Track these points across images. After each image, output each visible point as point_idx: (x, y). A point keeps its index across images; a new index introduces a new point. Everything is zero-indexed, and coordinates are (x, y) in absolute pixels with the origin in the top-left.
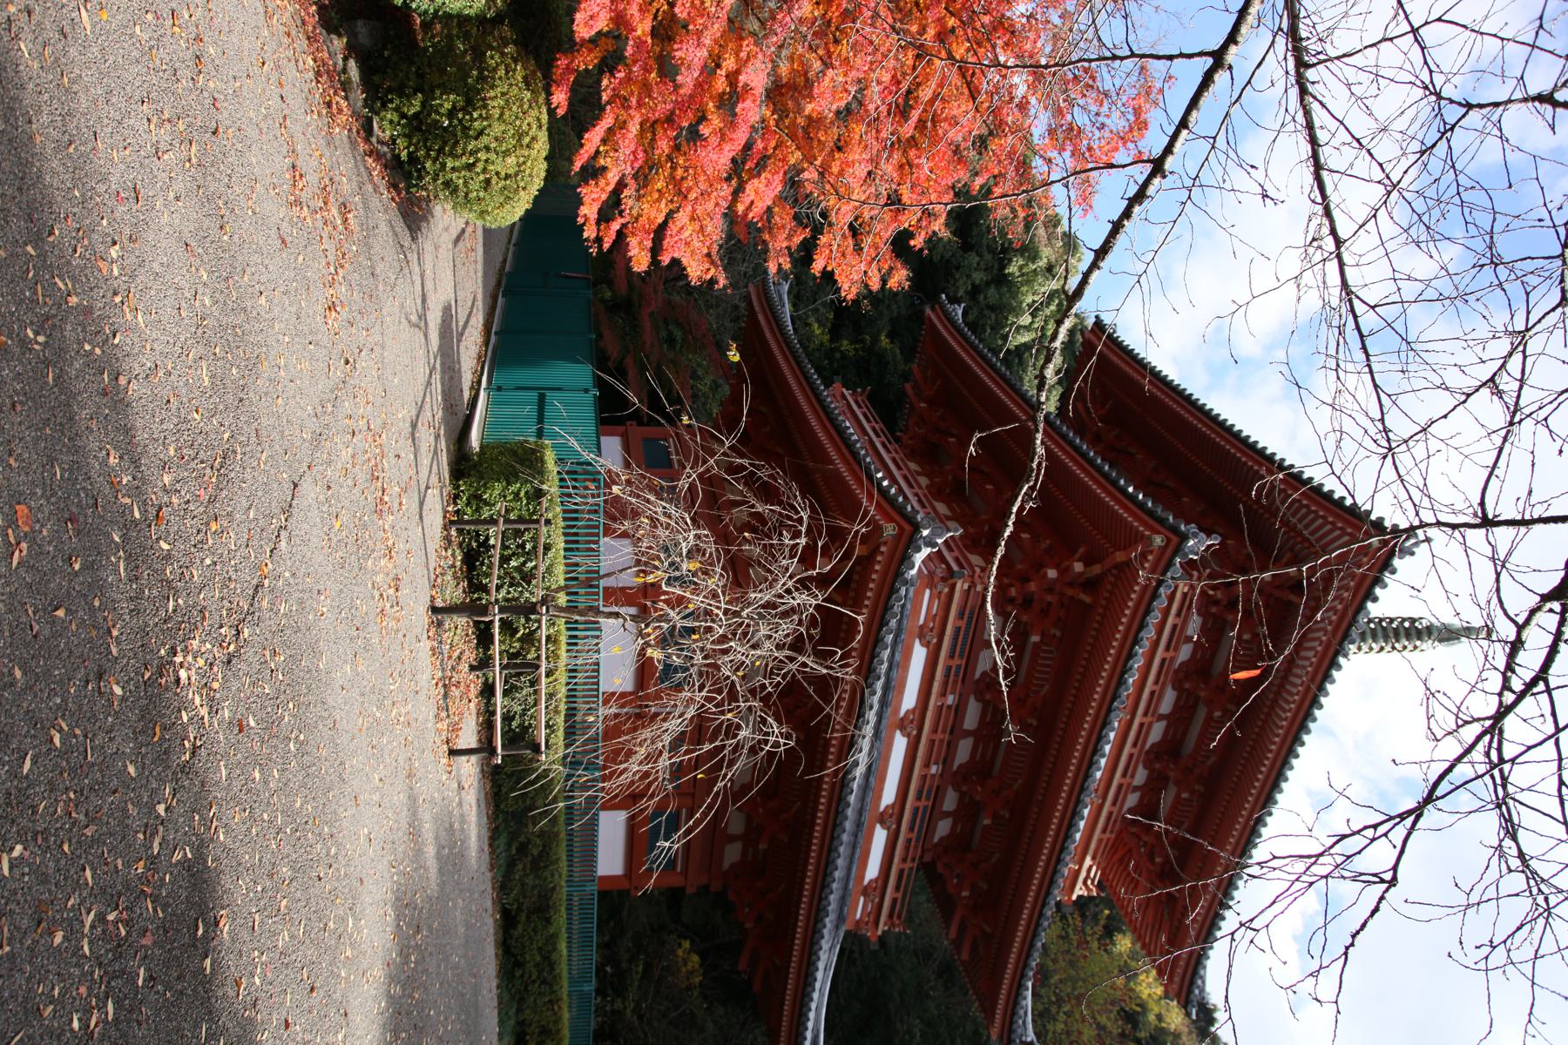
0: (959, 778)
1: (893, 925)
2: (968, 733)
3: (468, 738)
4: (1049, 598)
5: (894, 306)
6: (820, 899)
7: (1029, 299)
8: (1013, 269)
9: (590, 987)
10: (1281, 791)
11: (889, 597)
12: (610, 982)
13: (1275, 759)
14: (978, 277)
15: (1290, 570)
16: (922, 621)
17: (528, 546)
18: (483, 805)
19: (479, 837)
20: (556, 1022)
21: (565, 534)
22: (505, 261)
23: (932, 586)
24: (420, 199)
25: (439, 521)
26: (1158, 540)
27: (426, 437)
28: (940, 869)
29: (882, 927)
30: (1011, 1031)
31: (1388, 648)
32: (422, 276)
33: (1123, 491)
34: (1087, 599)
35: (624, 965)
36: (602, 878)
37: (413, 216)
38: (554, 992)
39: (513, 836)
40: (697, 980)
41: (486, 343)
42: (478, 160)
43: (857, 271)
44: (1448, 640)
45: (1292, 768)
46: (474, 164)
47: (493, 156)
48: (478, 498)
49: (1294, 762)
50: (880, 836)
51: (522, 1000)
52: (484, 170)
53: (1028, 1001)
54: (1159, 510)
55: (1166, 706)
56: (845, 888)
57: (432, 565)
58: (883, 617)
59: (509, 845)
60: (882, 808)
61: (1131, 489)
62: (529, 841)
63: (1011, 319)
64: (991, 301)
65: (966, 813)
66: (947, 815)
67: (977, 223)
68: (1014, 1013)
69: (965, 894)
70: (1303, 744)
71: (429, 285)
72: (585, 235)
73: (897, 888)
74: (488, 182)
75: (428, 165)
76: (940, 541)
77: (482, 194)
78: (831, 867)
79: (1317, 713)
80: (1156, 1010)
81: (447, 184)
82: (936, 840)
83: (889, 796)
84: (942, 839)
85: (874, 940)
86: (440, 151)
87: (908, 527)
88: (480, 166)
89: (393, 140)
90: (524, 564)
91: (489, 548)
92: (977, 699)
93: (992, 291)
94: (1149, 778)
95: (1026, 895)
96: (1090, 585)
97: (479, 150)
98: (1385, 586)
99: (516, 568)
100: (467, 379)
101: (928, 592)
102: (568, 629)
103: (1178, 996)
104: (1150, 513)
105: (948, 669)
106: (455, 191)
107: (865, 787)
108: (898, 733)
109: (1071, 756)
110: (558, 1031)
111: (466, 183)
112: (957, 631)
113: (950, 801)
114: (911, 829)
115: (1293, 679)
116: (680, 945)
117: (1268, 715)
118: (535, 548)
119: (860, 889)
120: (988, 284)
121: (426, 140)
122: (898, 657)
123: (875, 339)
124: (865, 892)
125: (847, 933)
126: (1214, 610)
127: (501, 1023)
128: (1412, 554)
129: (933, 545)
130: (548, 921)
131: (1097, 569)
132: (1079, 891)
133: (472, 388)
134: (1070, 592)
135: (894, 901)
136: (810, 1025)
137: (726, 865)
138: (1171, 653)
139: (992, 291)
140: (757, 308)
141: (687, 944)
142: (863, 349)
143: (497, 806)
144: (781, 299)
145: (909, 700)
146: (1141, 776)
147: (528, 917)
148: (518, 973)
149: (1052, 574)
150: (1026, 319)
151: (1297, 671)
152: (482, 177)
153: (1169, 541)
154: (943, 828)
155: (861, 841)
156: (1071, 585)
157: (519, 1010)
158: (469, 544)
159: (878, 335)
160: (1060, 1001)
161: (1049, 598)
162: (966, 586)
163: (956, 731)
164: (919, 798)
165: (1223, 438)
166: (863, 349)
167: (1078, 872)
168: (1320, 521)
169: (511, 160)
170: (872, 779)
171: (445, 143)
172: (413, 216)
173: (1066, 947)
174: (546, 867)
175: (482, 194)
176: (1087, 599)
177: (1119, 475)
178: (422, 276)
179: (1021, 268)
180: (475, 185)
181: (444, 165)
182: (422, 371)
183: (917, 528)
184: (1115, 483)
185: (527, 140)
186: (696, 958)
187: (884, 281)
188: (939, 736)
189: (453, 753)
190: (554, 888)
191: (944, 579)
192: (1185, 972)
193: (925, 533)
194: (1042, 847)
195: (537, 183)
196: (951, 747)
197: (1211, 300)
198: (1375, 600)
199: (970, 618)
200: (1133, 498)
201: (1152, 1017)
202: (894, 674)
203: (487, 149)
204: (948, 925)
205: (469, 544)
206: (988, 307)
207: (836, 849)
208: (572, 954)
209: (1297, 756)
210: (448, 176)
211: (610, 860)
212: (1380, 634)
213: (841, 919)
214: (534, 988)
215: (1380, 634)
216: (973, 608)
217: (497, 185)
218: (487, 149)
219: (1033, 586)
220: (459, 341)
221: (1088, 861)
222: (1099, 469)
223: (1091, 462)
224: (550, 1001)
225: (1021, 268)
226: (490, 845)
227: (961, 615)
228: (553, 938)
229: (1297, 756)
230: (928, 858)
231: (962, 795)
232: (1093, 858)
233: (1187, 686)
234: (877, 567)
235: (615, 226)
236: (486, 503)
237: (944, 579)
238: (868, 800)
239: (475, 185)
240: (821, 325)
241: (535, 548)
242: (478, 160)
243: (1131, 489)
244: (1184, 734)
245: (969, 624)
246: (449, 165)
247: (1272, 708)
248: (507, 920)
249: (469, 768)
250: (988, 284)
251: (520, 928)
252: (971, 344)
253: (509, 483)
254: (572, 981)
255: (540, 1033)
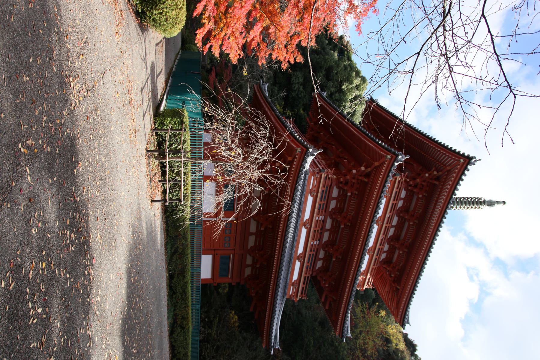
0: (325, 246)
1: (303, 297)
2: (327, 230)
3: (158, 197)
4: (354, 181)
5: (305, 100)
6: (277, 282)
7: (350, 98)
8: (344, 87)
9: (198, 307)
10: (433, 248)
11: (299, 173)
12: (206, 322)
13: (431, 237)
14: (333, 90)
15: (433, 174)
16: (311, 188)
17: (179, 141)
18: (163, 233)
19: (161, 238)
20: (187, 315)
21: (191, 140)
22: (172, 68)
23: (314, 175)
24: (145, 25)
25: (149, 128)
26: (389, 157)
27: (147, 116)
28: (319, 278)
29: (299, 298)
30: (343, 333)
31: (470, 208)
32: (145, 46)
33: (378, 143)
34: (366, 180)
35: (212, 319)
36: (203, 279)
37: (143, 28)
38: (186, 303)
39: (172, 246)
40: (237, 324)
41: (166, 86)
42: (163, 11)
43: (285, 56)
44: (491, 205)
45: (436, 240)
46: (162, 13)
47: (168, 10)
48: (162, 123)
49: (437, 238)
50: (298, 264)
51: (175, 306)
52: (166, 15)
53: (348, 322)
54: (389, 148)
55: (394, 223)
56: (286, 282)
57: (147, 138)
58: (297, 180)
59: (171, 248)
60: (298, 254)
61: (380, 142)
62: (178, 247)
63: (344, 104)
64: (337, 98)
65: (327, 258)
66: (320, 259)
67: (332, 72)
68: (343, 326)
69: (327, 285)
70: (440, 231)
71: (147, 51)
72: (198, 45)
73: (304, 283)
74: (167, 19)
75: (148, 13)
76: (316, 154)
77: (165, 23)
78: (281, 270)
79: (444, 220)
80: (395, 342)
81: (154, 20)
82: (317, 268)
83: (300, 250)
84: (319, 268)
85: (296, 302)
86: (152, 8)
87: (305, 149)
88: (164, 13)
89: (136, 5)
90: (177, 147)
91: (166, 141)
92: (330, 218)
93: (337, 94)
94: (389, 248)
95: (347, 283)
96: (367, 175)
97: (164, 8)
98: (465, 175)
99: (174, 148)
100: (160, 92)
101: (313, 177)
102: (191, 131)
103: (400, 322)
104: (386, 149)
105: (320, 205)
106: (156, 22)
107: (292, 246)
108: (303, 227)
109: (361, 236)
110: (188, 318)
111: (160, 19)
112: (323, 191)
113: (322, 254)
114: (308, 262)
115: (435, 213)
116: (231, 313)
117: (428, 223)
118: (180, 141)
119: (291, 283)
120: (336, 92)
121: (147, 4)
122: (303, 200)
123: (299, 110)
124: (293, 284)
125: (287, 299)
126: (410, 188)
127: (168, 313)
128: (474, 164)
129: (313, 155)
130: (184, 277)
131: (369, 169)
132: (366, 286)
133: (161, 96)
134: (360, 178)
135: (303, 288)
136: (274, 331)
137: (246, 276)
138: (382, 246)
139: (337, 94)
140: (257, 91)
141: (233, 312)
142: (294, 114)
143: (167, 234)
144: (265, 89)
145: (307, 216)
146: (386, 247)
147: (178, 275)
148: (174, 296)
149: (354, 171)
150: (349, 104)
151: (437, 207)
152: (165, 17)
153: (392, 157)
154: (319, 264)
155: (291, 266)
156: (361, 176)
157: (174, 310)
158: (159, 140)
159: (300, 109)
160: (361, 333)
161: (354, 181)
162: (325, 175)
163: (323, 229)
164: (311, 251)
165: (412, 132)
166: (294, 114)
167: (365, 279)
168: (444, 155)
169: (174, 13)
170: (295, 243)
171: (153, 5)
172: (143, 28)
173: (363, 315)
174: (184, 257)
175: (165, 23)
176: (366, 180)
177: (376, 138)
178: (145, 46)
179: (347, 87)
180: (163, 20)
181: (153, 13)
182: (145, 78)
183: (308, 149)
184: (375, 141)
185: (179, 7)
186: (236, 317)
187: (295, 59)
188: (317, 229)
189: (153, 201)
190: (186, 265)
191: (318, 173)
192: (402, 313)
193: (311, 150)
194: (352, 266)
195: (183, 23)
196: (322, 235)
197: (412, 97)
198: (462, 180)
199: (327, 187)
200: (380, 145)
201: (394, 345)
202: (302, 206)
203: (167, 8)
204: (321, 297)
205: (159, 140)
206: (336, 100)
207: (282, 264)
208: (193, 297)
209: (438, 236)
210: (154, 17)
211: (206, 273)
212: (467, 203)
213: (284, 294)
214: (180, 302)
215: (467, 203)
216: (328, 185)
217: (170, 21)
218: (167, 8)
219: (348, 177)
220: (157, 78)
221: (369, 276)
222: (370, 137)
223: (367, 135)
224: (185, 307)
225: (347, 87)
226: (165, 247)
227: (324, 186)
228: (187, 282)
229: (438, 236)
230: (314, 274)
231: (326, 252)
232: (370, 275)
233: (401, 215)
234: (295, 163)
235: (208, 46)
236: (165, 125)
237: (318, 173)
238: (294, 251)
239: (163, 20)
240: (280, 106)
241: (180, 141)
242: (163, 11)
243: (380, 142)
244: (411, 203)
245: (327, 189)
246: (154, 13)
247: (429, 220)
248: (171, 278)
249: (158, 205)
250: (336, 92)
251: (175, 279)
252: (329, 104)
253: (172, 119)
254: (192, 305)
255: (181, 319)
